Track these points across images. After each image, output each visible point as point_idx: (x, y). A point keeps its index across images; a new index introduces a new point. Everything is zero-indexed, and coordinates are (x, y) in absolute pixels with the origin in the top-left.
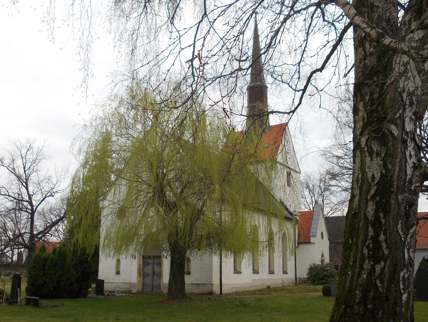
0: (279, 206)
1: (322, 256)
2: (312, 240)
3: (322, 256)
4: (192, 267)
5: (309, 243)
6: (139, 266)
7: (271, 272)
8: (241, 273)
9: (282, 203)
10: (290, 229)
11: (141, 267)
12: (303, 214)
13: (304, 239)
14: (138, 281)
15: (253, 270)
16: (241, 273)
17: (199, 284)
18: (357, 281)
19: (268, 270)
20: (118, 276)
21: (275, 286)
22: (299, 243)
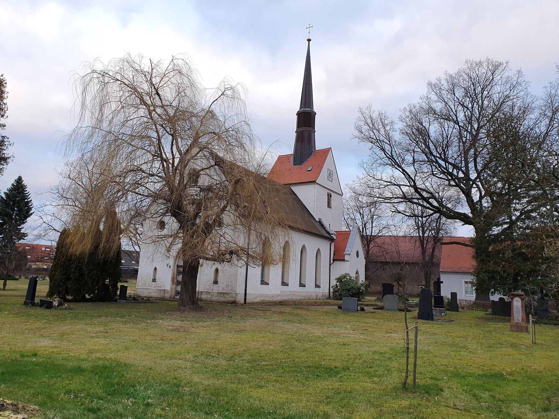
0: (317, 225)
1: (357, 273)
2: (346, 258)
3: (357, 273)
4: (213, 277)
5: (344, 260)
6: (173, 274)
7: (302, 285)
8: (268, 284)
9: (320, 222)
10: (325, 248)
11: (175, 276)
12: (339, 233)
13: (338, 256)
14: (171, 288)
15: (316, 284)
16: (268, 284)
17: (224, 293)
18: (478, 186)
19: (299, 283)
20: (154, 283)
21: (193, 314)
22: (334, 260)
